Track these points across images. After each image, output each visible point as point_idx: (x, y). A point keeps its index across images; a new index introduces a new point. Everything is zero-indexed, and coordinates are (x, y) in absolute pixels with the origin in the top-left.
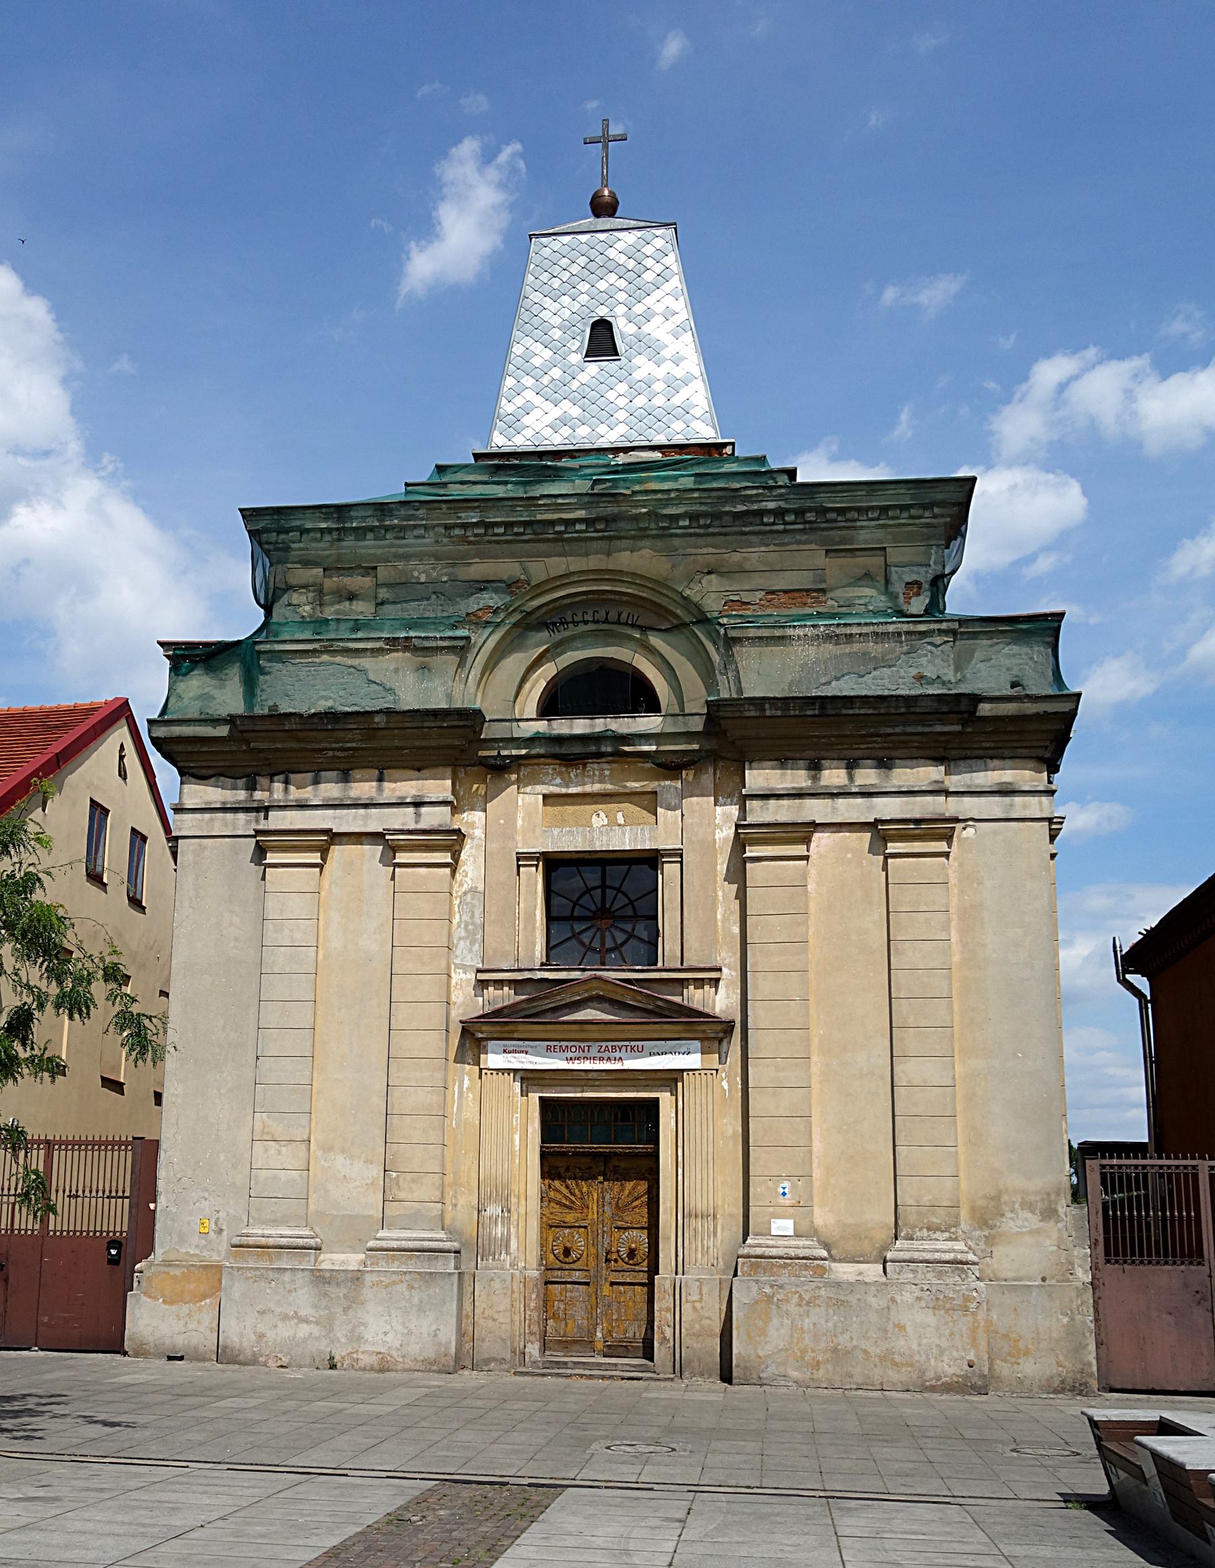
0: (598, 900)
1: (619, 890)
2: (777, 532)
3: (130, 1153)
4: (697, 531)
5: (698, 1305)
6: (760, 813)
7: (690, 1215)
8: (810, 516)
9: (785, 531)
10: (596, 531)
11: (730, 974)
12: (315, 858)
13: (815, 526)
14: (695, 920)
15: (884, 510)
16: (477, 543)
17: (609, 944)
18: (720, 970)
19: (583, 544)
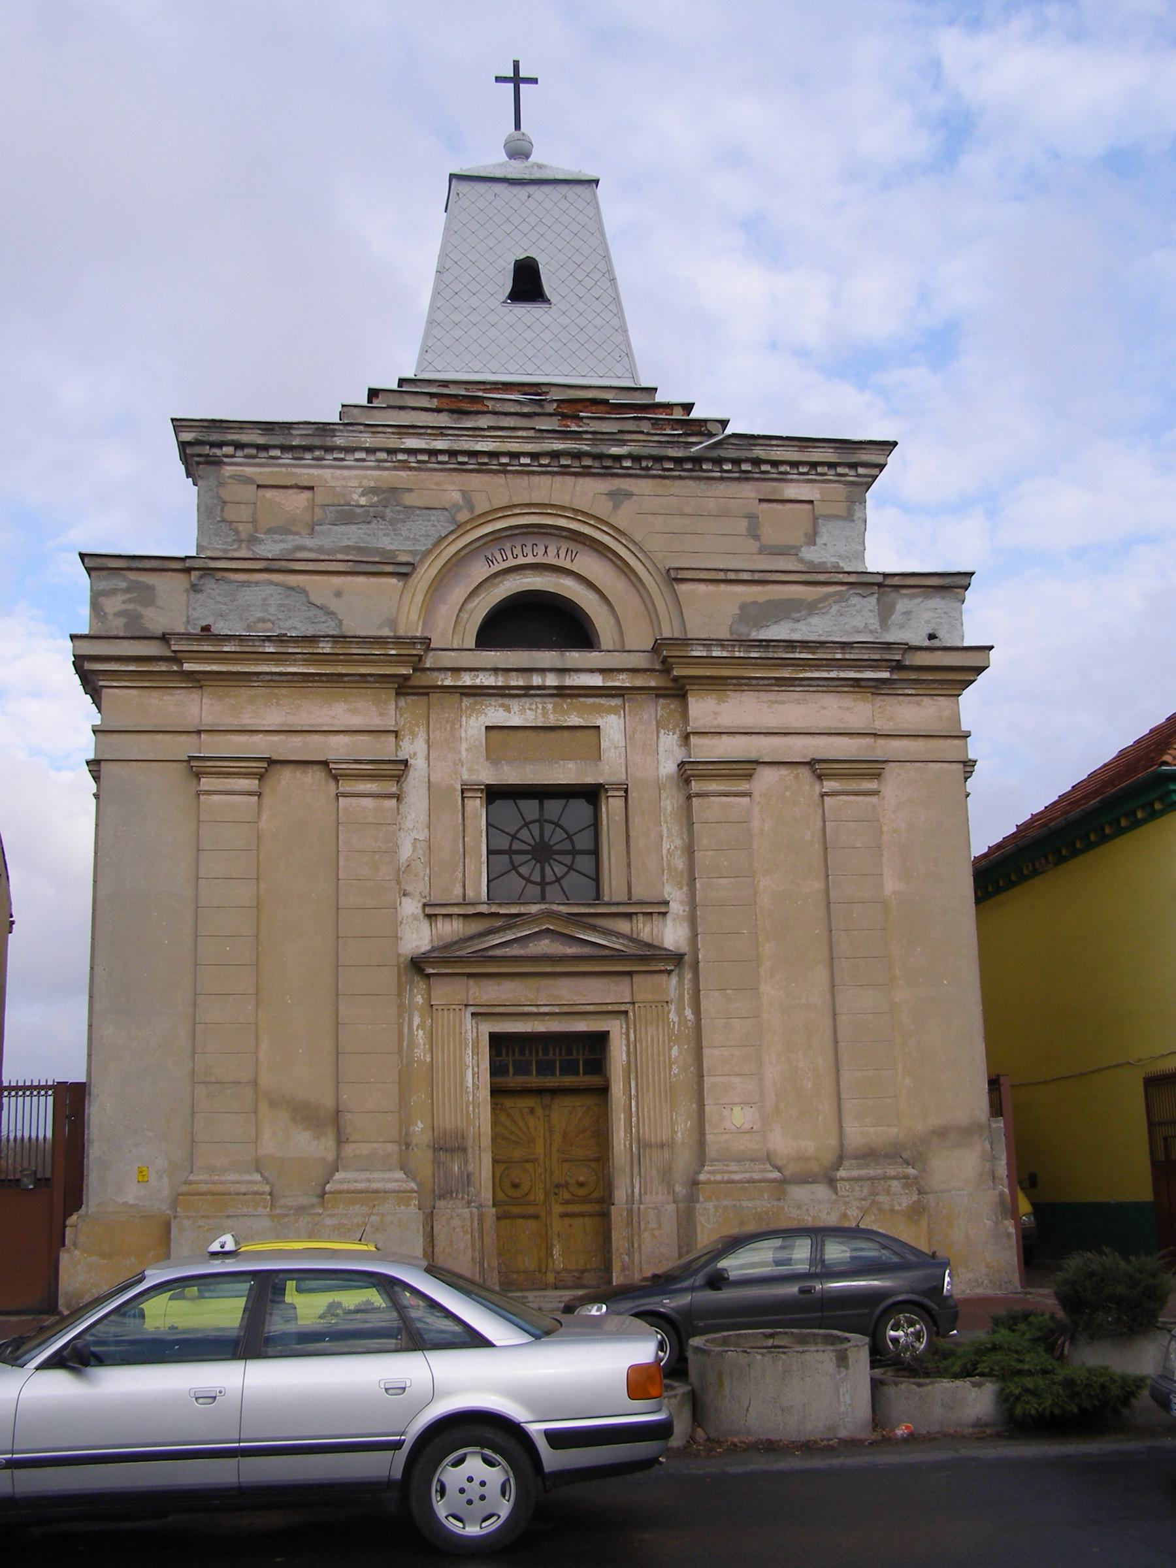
0: (536, 833)
1: (557, 824)
2: (714, 478)
3: (50, 1099)
4: (638, 472)
5: (657, 1233)
6: (708, 749)
7: (643, 1145)
8: (745, 467)
9: (722, 479)
10: (541, 465)
11: (677, 907)
12: (251, 784)
13: (750, 475)
14: (646, 852)
15: (814, 465)
16: (419, 469)
17: (524, 870)
18: (667, 903)
19: (526, 477)
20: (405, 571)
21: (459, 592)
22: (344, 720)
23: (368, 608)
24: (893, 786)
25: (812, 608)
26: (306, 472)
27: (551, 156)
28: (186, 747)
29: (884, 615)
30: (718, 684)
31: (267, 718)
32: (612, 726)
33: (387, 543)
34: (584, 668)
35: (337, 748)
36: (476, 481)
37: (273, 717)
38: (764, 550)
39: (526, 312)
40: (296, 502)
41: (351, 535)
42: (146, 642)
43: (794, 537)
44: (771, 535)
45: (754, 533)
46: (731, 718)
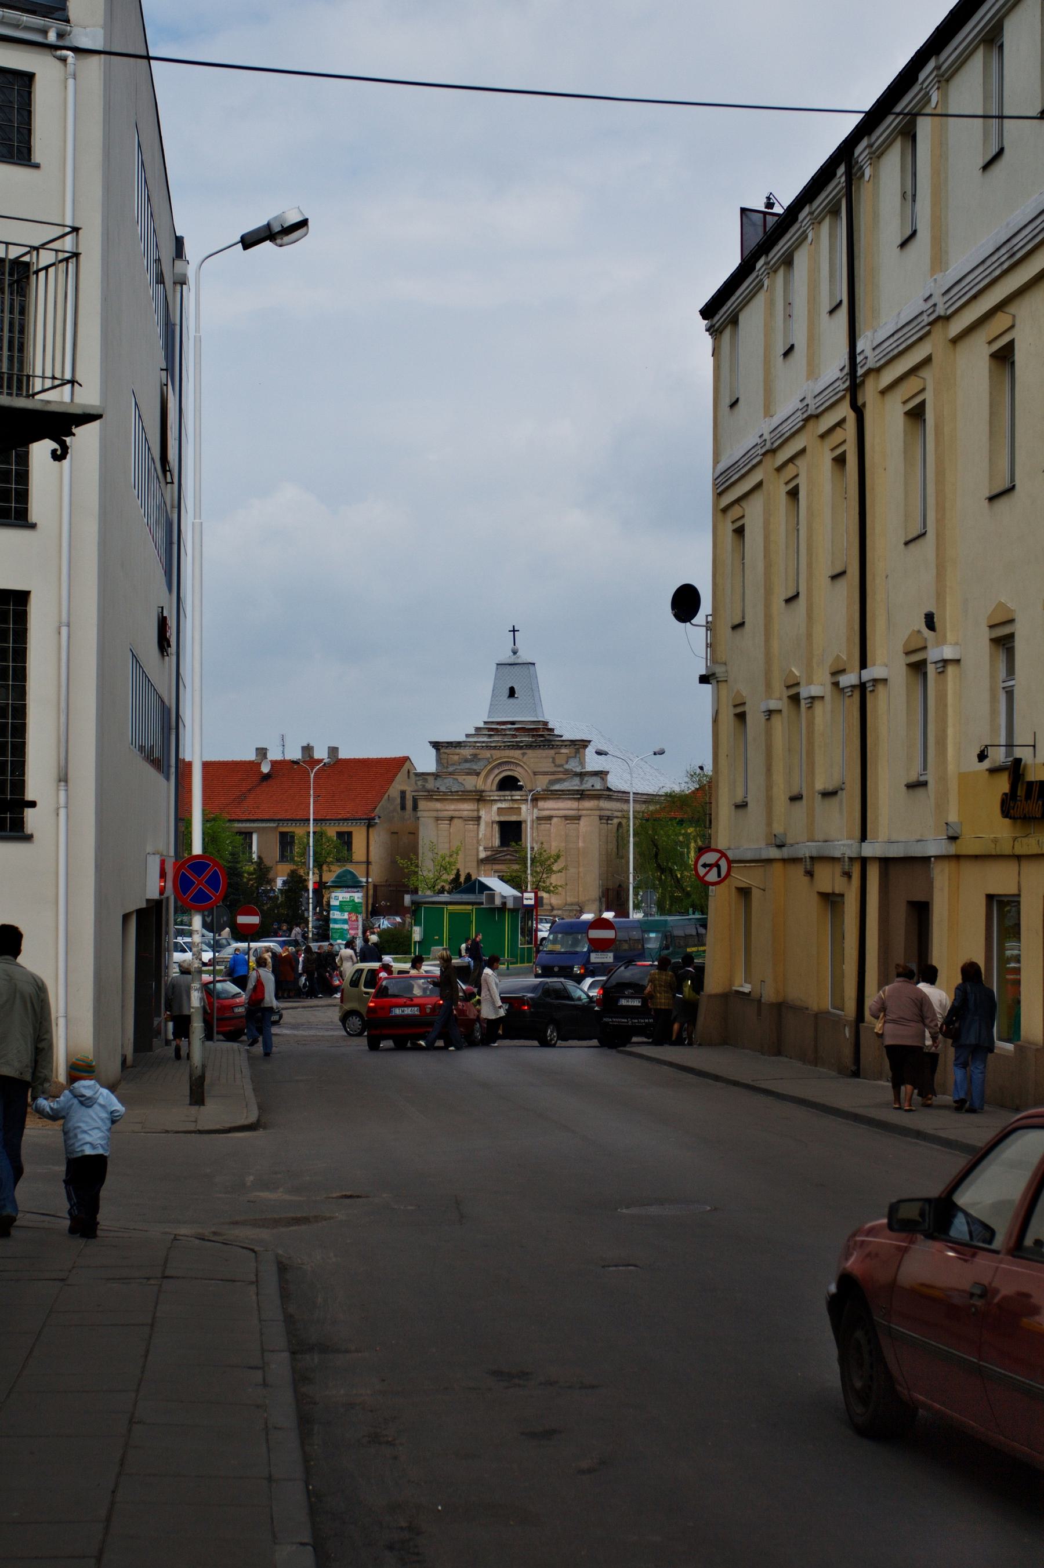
20: (478, 774)
21: (492, 777)
22: (467, 808)
23: (470, 783)
24: (582, 822)
25: (564, 780)
26: (457, 751)
27: (524, 656)
28: (435, 814)
29: (581, 781)
30: (544, 799)
31: (451, 808)
32: (524, 807)
33: (475, 767)
34: (517, 795)
35: (465, 813)
36: (493, 752)
37: (453, 807)
38: (556, 766)
39: (512, 700)
40: (456, 758)
41: (467, 765)
42: (1020, 226)
43: (563, 762)
44: (558, 762)
45: (553, 762)
46: (549, 806)
